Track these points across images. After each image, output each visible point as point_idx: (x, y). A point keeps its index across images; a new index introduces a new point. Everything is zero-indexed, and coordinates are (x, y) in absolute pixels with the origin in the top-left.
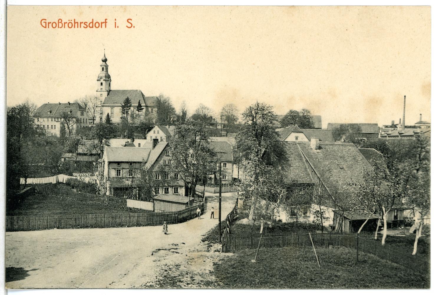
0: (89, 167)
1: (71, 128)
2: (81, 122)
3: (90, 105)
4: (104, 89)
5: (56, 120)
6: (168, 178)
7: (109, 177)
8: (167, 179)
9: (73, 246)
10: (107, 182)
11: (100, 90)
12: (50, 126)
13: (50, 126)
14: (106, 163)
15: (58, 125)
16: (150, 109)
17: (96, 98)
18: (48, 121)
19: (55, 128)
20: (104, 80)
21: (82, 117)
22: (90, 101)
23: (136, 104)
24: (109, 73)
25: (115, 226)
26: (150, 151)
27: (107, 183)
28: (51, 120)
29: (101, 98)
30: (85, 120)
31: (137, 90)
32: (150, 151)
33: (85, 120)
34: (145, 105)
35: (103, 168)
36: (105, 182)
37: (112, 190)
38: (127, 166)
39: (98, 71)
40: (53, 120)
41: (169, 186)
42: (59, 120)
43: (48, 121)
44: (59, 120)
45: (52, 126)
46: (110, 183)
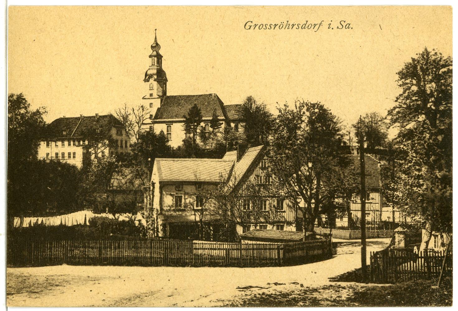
0: (132, 208)
1: (100, 155)
2: (117, 146)
3: (132, 118)
4: (155, 96)
5: (77, 143)
6: (265, 208)
7: (162, 209)
8: (263, 210)
9: (96, 280)
10: (159, 216)
11: (148, 96)
12: (66, 155)
13: (66, 155)
14: (157, 186)
15: (80, 151)
16: (233, 125)
17: (142, 107)
18: (63, 145)
19: (74, 157)
20: (155, 80)
21: (119, 138)
22: (132, 112)
23: (210, 117)
24: (164, 67)
25: (171, 264)
26: (234, 165)
27: (159, 220)
28: (68, 144)
29: (150, 109)
30: (124, 142)
31: (211, 95)
32: (234, 165)
33: (124, 142)
34: (223, 118)
35: (151, 196)
36: (156, 218)
37: (168, 228)
38: (190, 189)
39: (146, 64)
40: (72, 143)
41: (267, 222)
42: (81, 143)
43: (63, 145)
44: (81, 143)
45: (69, 154)
46: (163, 218)
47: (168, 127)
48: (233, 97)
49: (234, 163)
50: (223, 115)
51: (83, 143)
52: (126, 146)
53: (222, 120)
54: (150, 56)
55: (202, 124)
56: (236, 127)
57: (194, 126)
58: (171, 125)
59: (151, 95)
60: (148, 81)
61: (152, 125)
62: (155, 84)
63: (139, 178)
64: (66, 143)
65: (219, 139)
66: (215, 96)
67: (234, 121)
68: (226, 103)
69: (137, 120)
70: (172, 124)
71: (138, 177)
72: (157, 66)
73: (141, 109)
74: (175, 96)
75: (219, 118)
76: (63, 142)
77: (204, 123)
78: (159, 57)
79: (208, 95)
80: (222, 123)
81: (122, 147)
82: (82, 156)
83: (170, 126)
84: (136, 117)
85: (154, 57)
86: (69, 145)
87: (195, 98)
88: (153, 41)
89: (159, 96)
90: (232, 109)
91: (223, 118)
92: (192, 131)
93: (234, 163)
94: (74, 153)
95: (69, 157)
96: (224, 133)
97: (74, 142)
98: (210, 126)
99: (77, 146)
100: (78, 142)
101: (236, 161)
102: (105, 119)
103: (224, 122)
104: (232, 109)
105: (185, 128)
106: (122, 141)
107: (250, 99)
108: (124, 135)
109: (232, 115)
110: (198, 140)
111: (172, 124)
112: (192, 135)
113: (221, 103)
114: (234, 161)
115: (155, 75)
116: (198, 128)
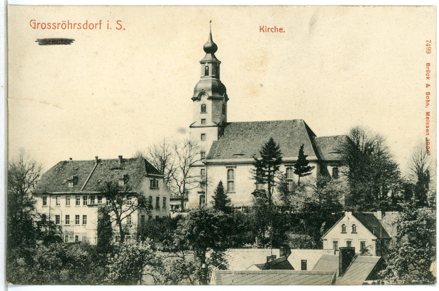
1: (124, 222)
4: (209, 122)
5: (89, 201)
11: (199, 123)
13: (72, 218)
15: (93, 215)
16: (330, 169)
19: (84, 222)
21: (154, 194)
22: (174, 152)
39: (195, 76)
40: (81, 201)
45: (77, 217)
47: (229, 170)
48: (331, 126)
49: (335, 277)
50: (314, 154)
51: (99, 202)
52: (164, 207)
53: (313, 161)
54: (202, 63)
55: (283, 168)
56: (336, 171)
57: (270, 171)
58: (234, 169)
59: (203, 120)
60: (200, 100)
61: (205, 168)
62: (209, 104)
63: (186, 278)
64: (73, 201)
65: (309, 195)
66: (301, 124)
67: (331, 163)
68: (319, 133)
69: (181, 164)
70: (236, 167)
71: (185, 276)
72: (213, 77)
73: (188, 147)
74: (239, 123)
75: (307, 158)
76: (68, 199)
77: (285, 166)
78: (216, 64)
79: (291, 121)
80: (314, 167)
81: (158, 207)
82: (97, 223)
83: (233, 170)
84: (180, 159)
85: (208, 63)
86: (77, 203)
87: (270, 126)
88: (207, 39)
89: (215, 123)
90: (328, 144)
91: (315, 158)
92: (266, 180)
93: (335, 277)
94: (85, 217)
95: (77, 222)
96: (316, 186)
97: (85, 198)
98: (294, 171)
99: (89, 206)
100: (91, 200)
101: (338, 275)
102: (133, 164)
103: (315, 165)
104: (328, 144)
105: (255, 175)
106: (158, 199)
107: (355, 132)
108: (161, 189)
109: (328, 154)
110: (276, 196)
111: (236, 167)
112: (266, 186)
113: (311, 134)
114: (334, 273)
115: (209, 90)
116: (275, 175)
